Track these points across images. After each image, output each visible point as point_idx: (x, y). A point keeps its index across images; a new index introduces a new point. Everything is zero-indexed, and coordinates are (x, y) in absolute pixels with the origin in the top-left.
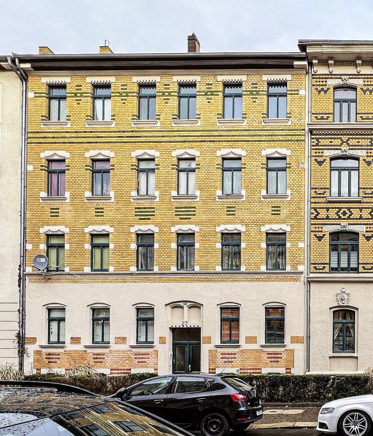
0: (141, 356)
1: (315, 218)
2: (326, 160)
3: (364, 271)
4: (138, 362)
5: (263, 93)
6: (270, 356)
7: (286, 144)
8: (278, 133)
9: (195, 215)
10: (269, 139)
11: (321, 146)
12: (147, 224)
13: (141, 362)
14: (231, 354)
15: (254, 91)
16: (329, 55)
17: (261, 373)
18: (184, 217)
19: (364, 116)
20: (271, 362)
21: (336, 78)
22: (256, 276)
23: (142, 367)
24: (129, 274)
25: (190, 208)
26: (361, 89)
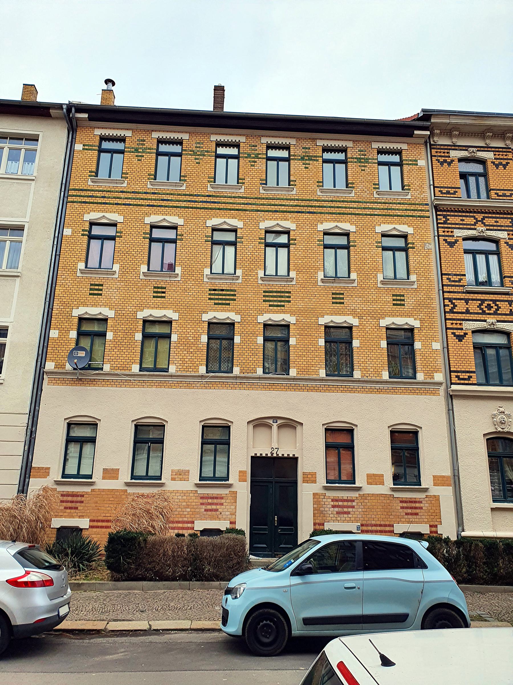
0: (210, 501)
1: (452, 311)
2: (458, 240)
3: (458, 382)
4: (206, 510)
5: (93, 148)
6: (405, 505)
7: (383, 219)
8: (394, 206)
9: (289, 302)
10: (383, 213)
11: (450, 224)
12: (225, 311)
13: (211, 510)
14: (347, 501)
15: (362, 159)
16: (454, 126)
17: (193, 528)
18: (275, 303)
19: (500, 193)
20: (407, 514)
21: (461, 150)
22: (378, 386)
23: (212, 518)
24: (199, 376)
25: (283, 292)
26: (492, 162)
